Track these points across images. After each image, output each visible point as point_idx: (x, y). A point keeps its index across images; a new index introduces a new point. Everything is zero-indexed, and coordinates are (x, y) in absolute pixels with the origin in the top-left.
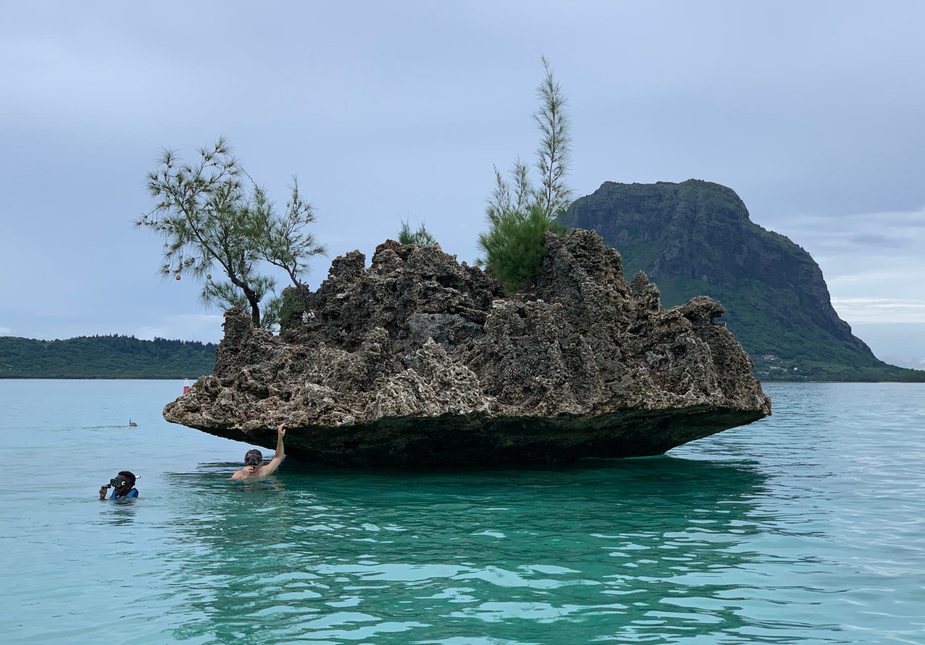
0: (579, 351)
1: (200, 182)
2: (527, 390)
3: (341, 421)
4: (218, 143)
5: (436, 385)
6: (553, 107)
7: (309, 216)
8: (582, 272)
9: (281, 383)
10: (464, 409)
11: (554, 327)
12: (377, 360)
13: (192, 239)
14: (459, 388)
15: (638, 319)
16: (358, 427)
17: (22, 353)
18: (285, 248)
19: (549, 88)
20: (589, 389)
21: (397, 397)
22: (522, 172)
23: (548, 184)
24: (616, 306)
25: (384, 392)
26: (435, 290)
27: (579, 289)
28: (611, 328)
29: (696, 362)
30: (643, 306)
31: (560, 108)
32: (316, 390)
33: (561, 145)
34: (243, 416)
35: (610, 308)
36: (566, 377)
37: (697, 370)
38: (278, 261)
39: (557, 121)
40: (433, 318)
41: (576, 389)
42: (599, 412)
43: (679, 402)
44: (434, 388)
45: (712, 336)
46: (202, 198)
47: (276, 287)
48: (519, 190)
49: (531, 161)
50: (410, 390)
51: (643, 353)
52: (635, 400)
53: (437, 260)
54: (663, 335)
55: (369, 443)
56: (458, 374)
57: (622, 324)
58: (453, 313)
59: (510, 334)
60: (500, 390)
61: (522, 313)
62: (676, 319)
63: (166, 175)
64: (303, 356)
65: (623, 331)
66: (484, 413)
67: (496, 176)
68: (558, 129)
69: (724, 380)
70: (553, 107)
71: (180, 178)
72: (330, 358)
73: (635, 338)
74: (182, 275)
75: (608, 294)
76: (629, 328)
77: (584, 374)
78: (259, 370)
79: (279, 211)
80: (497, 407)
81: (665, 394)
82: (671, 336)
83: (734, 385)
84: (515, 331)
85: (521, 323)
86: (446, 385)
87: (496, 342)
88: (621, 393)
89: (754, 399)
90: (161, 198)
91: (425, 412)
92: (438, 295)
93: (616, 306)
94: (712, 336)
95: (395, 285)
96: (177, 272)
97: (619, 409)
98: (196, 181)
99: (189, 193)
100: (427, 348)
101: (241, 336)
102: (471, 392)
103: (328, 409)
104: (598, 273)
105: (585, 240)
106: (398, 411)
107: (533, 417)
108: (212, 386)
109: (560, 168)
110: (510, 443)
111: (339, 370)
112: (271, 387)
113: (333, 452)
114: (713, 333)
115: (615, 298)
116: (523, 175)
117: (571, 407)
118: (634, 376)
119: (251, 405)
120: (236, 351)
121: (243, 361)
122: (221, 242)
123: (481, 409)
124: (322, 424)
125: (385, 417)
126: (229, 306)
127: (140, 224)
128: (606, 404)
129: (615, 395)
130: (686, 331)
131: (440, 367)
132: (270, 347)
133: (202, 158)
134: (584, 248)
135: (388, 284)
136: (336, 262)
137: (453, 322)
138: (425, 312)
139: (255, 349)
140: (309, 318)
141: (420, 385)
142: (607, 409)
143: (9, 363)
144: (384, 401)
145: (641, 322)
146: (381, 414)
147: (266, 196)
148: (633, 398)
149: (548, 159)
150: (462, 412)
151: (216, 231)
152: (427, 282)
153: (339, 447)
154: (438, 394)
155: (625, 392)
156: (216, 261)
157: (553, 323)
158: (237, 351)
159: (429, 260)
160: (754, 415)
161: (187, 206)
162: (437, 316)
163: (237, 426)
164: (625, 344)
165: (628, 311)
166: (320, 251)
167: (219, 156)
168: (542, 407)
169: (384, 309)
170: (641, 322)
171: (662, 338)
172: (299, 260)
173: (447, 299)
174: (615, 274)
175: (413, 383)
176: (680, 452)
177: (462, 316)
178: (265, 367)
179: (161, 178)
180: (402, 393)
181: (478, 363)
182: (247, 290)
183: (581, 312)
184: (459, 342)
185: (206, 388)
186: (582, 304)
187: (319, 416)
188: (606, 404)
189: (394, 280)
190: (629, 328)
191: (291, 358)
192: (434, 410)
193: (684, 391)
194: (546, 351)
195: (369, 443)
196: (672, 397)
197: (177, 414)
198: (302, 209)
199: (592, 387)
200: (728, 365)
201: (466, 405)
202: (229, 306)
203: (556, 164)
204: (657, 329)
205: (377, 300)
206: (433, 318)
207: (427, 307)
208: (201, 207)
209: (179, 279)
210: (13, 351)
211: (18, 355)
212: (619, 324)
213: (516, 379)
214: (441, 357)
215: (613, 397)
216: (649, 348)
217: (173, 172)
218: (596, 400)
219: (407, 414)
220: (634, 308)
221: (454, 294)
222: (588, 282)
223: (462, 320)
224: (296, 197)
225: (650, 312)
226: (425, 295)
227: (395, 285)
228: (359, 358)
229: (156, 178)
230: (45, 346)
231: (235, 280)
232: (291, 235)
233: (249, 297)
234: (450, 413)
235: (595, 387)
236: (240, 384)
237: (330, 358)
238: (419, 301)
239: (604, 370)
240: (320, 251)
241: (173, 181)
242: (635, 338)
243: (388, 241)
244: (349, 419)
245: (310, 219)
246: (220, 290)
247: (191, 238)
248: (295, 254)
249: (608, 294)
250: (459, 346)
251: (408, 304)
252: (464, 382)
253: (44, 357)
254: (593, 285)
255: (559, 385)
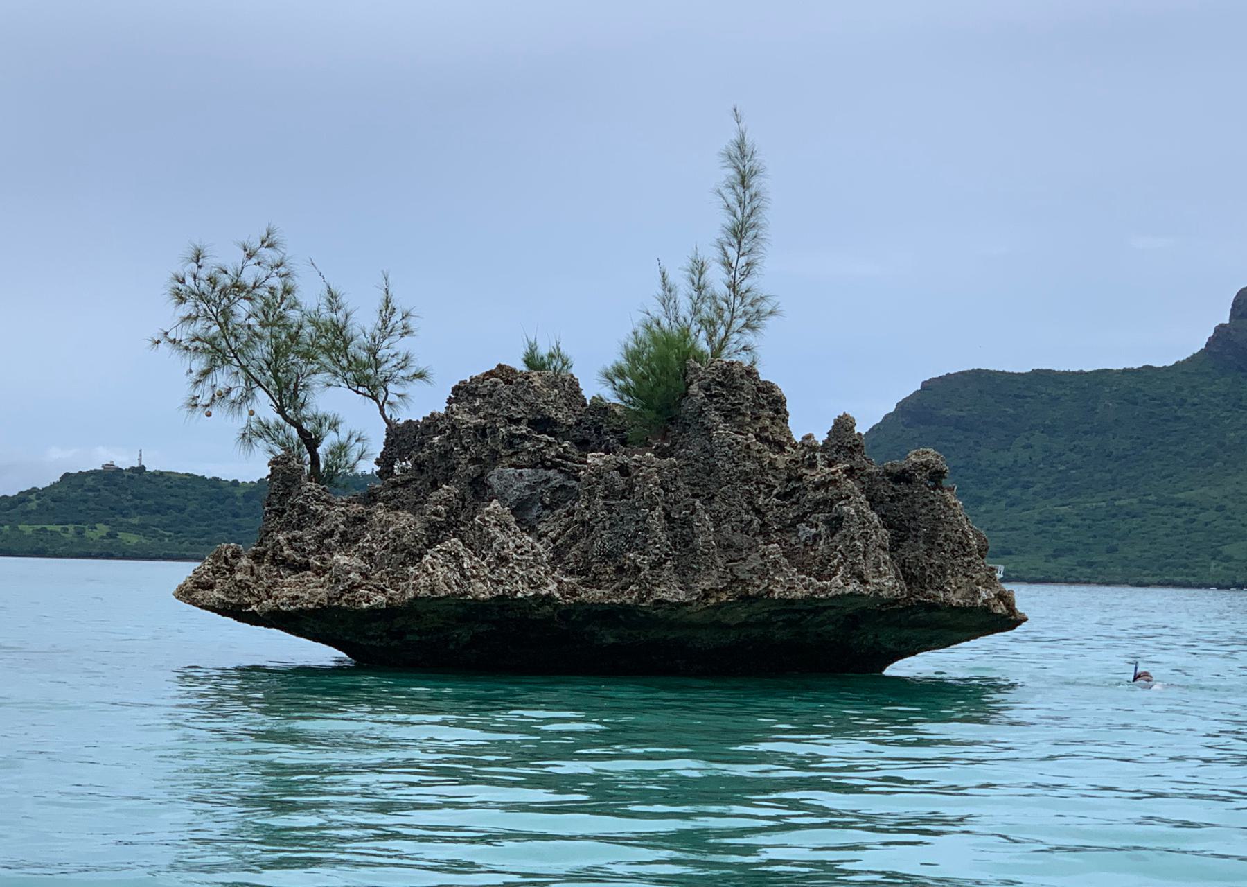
0: (691, 521)
1: (238, 287)
2: (620, 570)
3: (368, 602)
4: (264, 234)
5: (514, 563)
6: (744, 180)
7: (404, 327)
8: (714, 416)
9: (326, 555)
10: (523, 591)
11: (656, 490)
12: (442, 528)
13: (230, 362)
14: (518, 565)
15: (789, 480)
16: (389, 612)
17: (192, 506)
18: (371, 372)
19: (741, 153)
20: (699, 571)
21: (436, 574)
22: (699, 268)
23: (733, 286)
24: (760, 463)
25: (419, 568)
26: (523, 437)
27: (710, 440)
28: (749, 491)
29: (853, 539)
30: (797, 462)
31: (755, 183)
32: (342, 562)
33: (751, 233)
34: (263, 595)
35: (750, 466)
36: (667, 554)
37: (853, 549)
38: (361, 389)
39: (748, 200)
40: (521, 474)
41: (681, 570)
42: (713, 601)
43: (822, 590)
44: (489, 564)
45: (926, 505)
46: (242, 309)
47: (340, 427)
48: (695, 297)
49: (711, 256)
50: (453, 566)
51: (793, 525)
52: (758, 586)
53: (530, 398)
54: (818, 503)
55: (419, 632)
56: (518, 547)
57: (768, 486)
58: (550, 468)
59: (605, 498)
60: (589, 569)
61: (623, 470)
62: (836, 481)
63: (195, 277)
64: (362, 520)
65: (767, 496)
66: (549, 596)
67: (660, 275)
68: (748, 211)
69: (931, 565)
70: (744, 180)
71: (212, 281)
72: (388, 524)
73: (783, 506)
74: (214, 411)
75: (748, 446)
76: (775, 492)
77: (694, 551)
78: (301, 538)
79: (363, 323)
80: (575, 590)
81: (803, 580)
82: (828, 503)
83: (944, 572)
84: (610, 493)
85: (620, 483)
86: (503, 560)
87: (587, 508)
88: (742, 577)
89: (976, 592)
90: (187, 308)
91: (470, 593)
92: (528, 444)
93: (760, 463)
94: (926, 505)
95: (484, 429)
96: (207, 406)
97: (739, 598)
98: (235, 286)
99: (225, 301)
100: (489, 513)
101: (290, 493)
102: (534, 570)
103: (353, 587)
104: (740, 418)
105: (724, 374)
106: (433, 591)
107: (621, 604)
108: (233, 557)
109: (748, 265)
110: (612, 640)
111: (394, 540)
112: (312, 560)
113: (374, 643)
114: (926, 500)
115: (759, 451)
116: (701, 274)
117: (670, 592)
118: (762, 556)
119: (276, 582)
120: (281, 513)
121: (287, 526)
122: (269, 364)
123: (544, 592)
124: (344, 605)
125: (416, 598)
126: (279, 452)
127: (158, 342)
128: (723, 590)
129: (736, 580)
130: (848, 497)
131: (502, 537)
132: (321, 508)
133: (243, 254)
134: (721, 384)
135: (476, 426)
136: (456, 390)
137: (548, 481)
138: (511, 466)
139: (303, 509)
140: (403, 470)
141: (466, 560)
142: (724, 597)
143: (164, 527)
144: (416, 578)
145: (794, 484)
146: (411, 594)
147: (343, 300)
148: (757, 583)
149: (733, 253)
150: (519, 595)
151: (262, 351)
152: (513, 427)
153: (381, 637)
154: (492, 572)
155: (747, 576)
156: (260, 393)
157: (655, 484)
158: (284, 511)
159: (518, 398)
160: (1009, 620)
161: (221, 319)
162: (525, 471)
163: (254, 607)
164: (770, 514)
165: (776, 469)
166: (420, 375)
167: (266, 253)
168: (632, 592)
169: (470, 461)
170: (794, 484)
171: (817, 506)
172: (391, 387)
173: (539, 449)
174: (773, 419)
175: (457, 557)
176: (901, 668)
177: (561, 472)
178: (308, 536)
179: (189, 281)
180: (440, 569)
181: (575, 534)
182: (301, 431)
183: (711, 470)
184: (558, 507)
185: (226, 560)
186: (712, 460)
187: (342, 595)
188: (723, 590)
189: (484, 422)
190: (775, 492)
191: (343, 523)
192: (482, 590)
193: (830, 577)
194: (644, 521)
195: (419, 632)
196: (811, 584)
197: (185, 594)
198: (397, 317)
199: (703, 568)
200: (940, 545)
201: (525, 586)
202: (279, 452)
203: (743, 261)
204: (810, 495)
205: (466, 449)
206: (521, 474)
207: (514, 459)
208: (239, 320)
209: (209, 415)
210: (172, 501)
211: (181, 510)
212: (762, 486)
213: (608, 556)
214: (507, 526)
215: (733, 581)
216: (801, 519)
217: (203, 274)
218: (706, 584)
219: (443, 594)
220: (783, 466)
221: (549, 444)
222: (723, 431)
223: (560, 477)
224: (387, 301)
225: (805, 471)
226: (511, 445)
227: (484, 429)
228: (418, 525)
229: (183, 282)
230: (239, 493)
231: (285, 418)
232: (380, 353)
233: (304, 441)
234: (504, 595)
235: (708, 568)
236: (274, 555)
237: (388, 524)
238: (503, 452)
239: (730, 546)
240: (420, 375)
241: (204, 286)
242: (783, 506)
243: (500, 366)
244: (380, 598)
245: (406, 331)
246: (265, 430)
247: (226, 362)
248: (385, 381)
249: (748, 446)
250: (557, 512)
251: (495, 457)
252: (525, 557)
253: (236, 516)
254: (728, 435)
255: (657, 565)
